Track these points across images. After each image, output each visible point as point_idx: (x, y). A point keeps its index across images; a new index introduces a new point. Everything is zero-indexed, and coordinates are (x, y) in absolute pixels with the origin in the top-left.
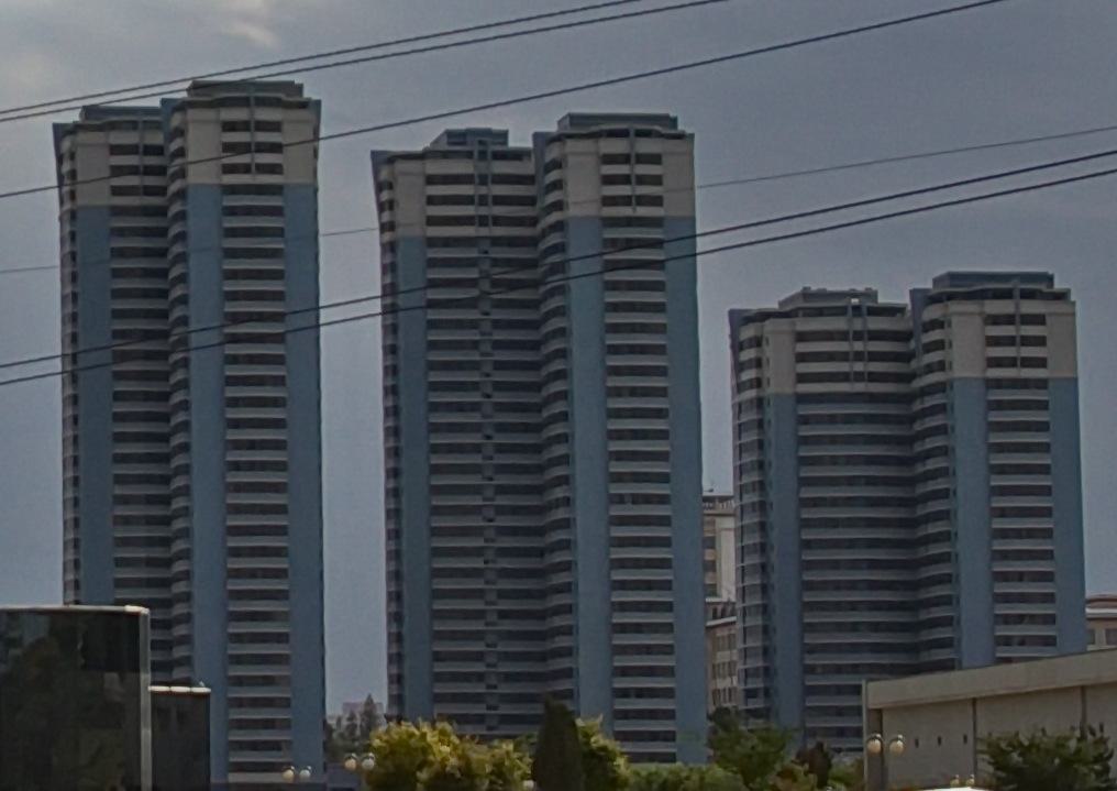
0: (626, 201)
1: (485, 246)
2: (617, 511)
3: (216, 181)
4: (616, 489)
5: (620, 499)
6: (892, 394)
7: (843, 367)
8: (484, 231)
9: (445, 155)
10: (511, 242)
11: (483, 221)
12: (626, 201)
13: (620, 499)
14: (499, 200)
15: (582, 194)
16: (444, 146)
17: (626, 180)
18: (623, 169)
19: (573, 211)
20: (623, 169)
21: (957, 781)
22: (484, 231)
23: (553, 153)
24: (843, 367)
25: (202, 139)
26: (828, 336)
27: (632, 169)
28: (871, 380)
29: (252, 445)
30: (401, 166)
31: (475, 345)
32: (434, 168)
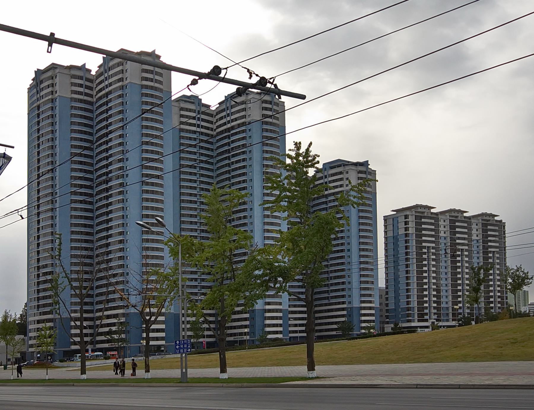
8: (198, 130)
22: (198, 130)
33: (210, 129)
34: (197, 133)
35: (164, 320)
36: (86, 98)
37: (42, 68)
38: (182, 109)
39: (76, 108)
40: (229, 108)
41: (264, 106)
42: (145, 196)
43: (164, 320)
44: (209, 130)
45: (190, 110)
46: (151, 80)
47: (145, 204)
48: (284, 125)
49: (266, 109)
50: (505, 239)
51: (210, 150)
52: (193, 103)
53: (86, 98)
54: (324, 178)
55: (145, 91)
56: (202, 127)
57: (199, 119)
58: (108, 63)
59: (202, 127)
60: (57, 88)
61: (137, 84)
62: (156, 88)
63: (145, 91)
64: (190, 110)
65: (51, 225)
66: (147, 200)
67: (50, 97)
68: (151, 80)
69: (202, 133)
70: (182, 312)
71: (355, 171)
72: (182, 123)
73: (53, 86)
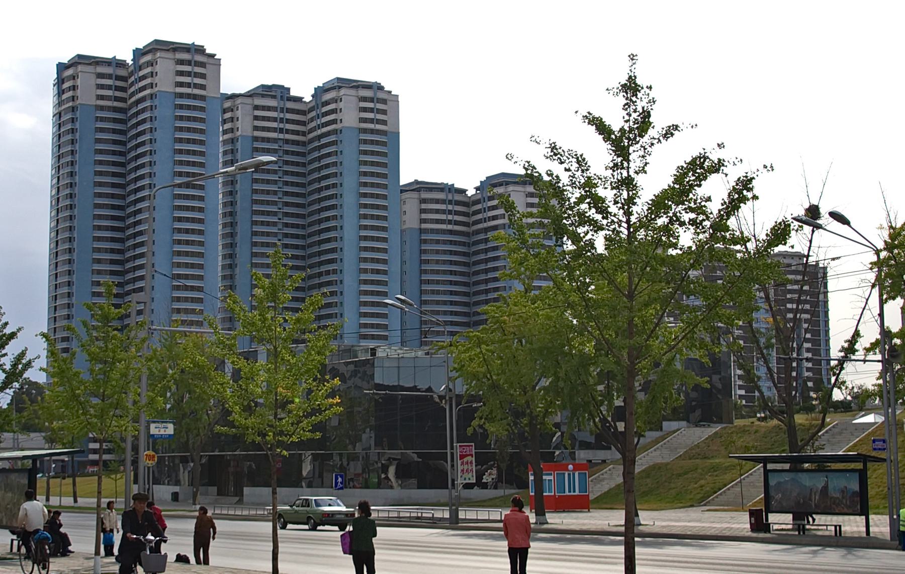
0: (371, 121)
1: (281, 143)
2: (364, 277)
3: (172, 90)
4: (363, 266)
5: (365, 271)
6: (463, 232)
7: (443, 217)
8: (281, 136)
9: (263, 96)
10: (294, 143)
11: (281, 131)
12: (371, 121)
13: (365, 271)
14: (288, 121)
15: (349, 117)
16: (260, 91)
17: (371, 110)
18: (371, 105)
19: (346, 124)
20: (371, 105)
21: (223, 438)
22: (281, 136)
23: (328, 96)
24: (443, 217)
25: (165, 68)
26: (437, 201)
27: (375, 105)
28: (455, 224)
29: (187, 231)
30: (239, 101)
31: (275, 193)
32: (259, 102)
33: (301, 133)
34: (279, 141)
35: (664, 423)
36: (116, 104)
37: (65, 61)
38: (256, 108)
39: (102, 119)
40: (320, 106)
41: (361, 106)
42: (177, 248)
43: (664, 423)
44: (298, 135)
45: (269, 108)
46: (188, 85)
47: (177, 260)
48: (396, 131)
49: (364, 110)
50: (826, 296)
51: (301, 164)
52: (274, 97)
53: (116, 104)
54: (482, 201)
55: (179, 102)
56: (287, 131)
57: (282, 119)
58: (139, 60)
59: (287, 131)
60: (79, 92)
61: (167, 92)
62: (195, 95)
63: (179, 102)
64: (269, 108)
65: (67, 283)
66: (179, 253)
67: (70, 104)
68: (188, 85)
69: (287, 141)
70: (148, 428)
71: (522, 193)
72: (256, 128)
73: (74, 89)
